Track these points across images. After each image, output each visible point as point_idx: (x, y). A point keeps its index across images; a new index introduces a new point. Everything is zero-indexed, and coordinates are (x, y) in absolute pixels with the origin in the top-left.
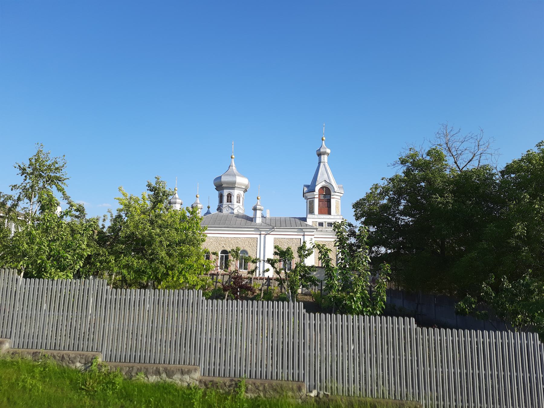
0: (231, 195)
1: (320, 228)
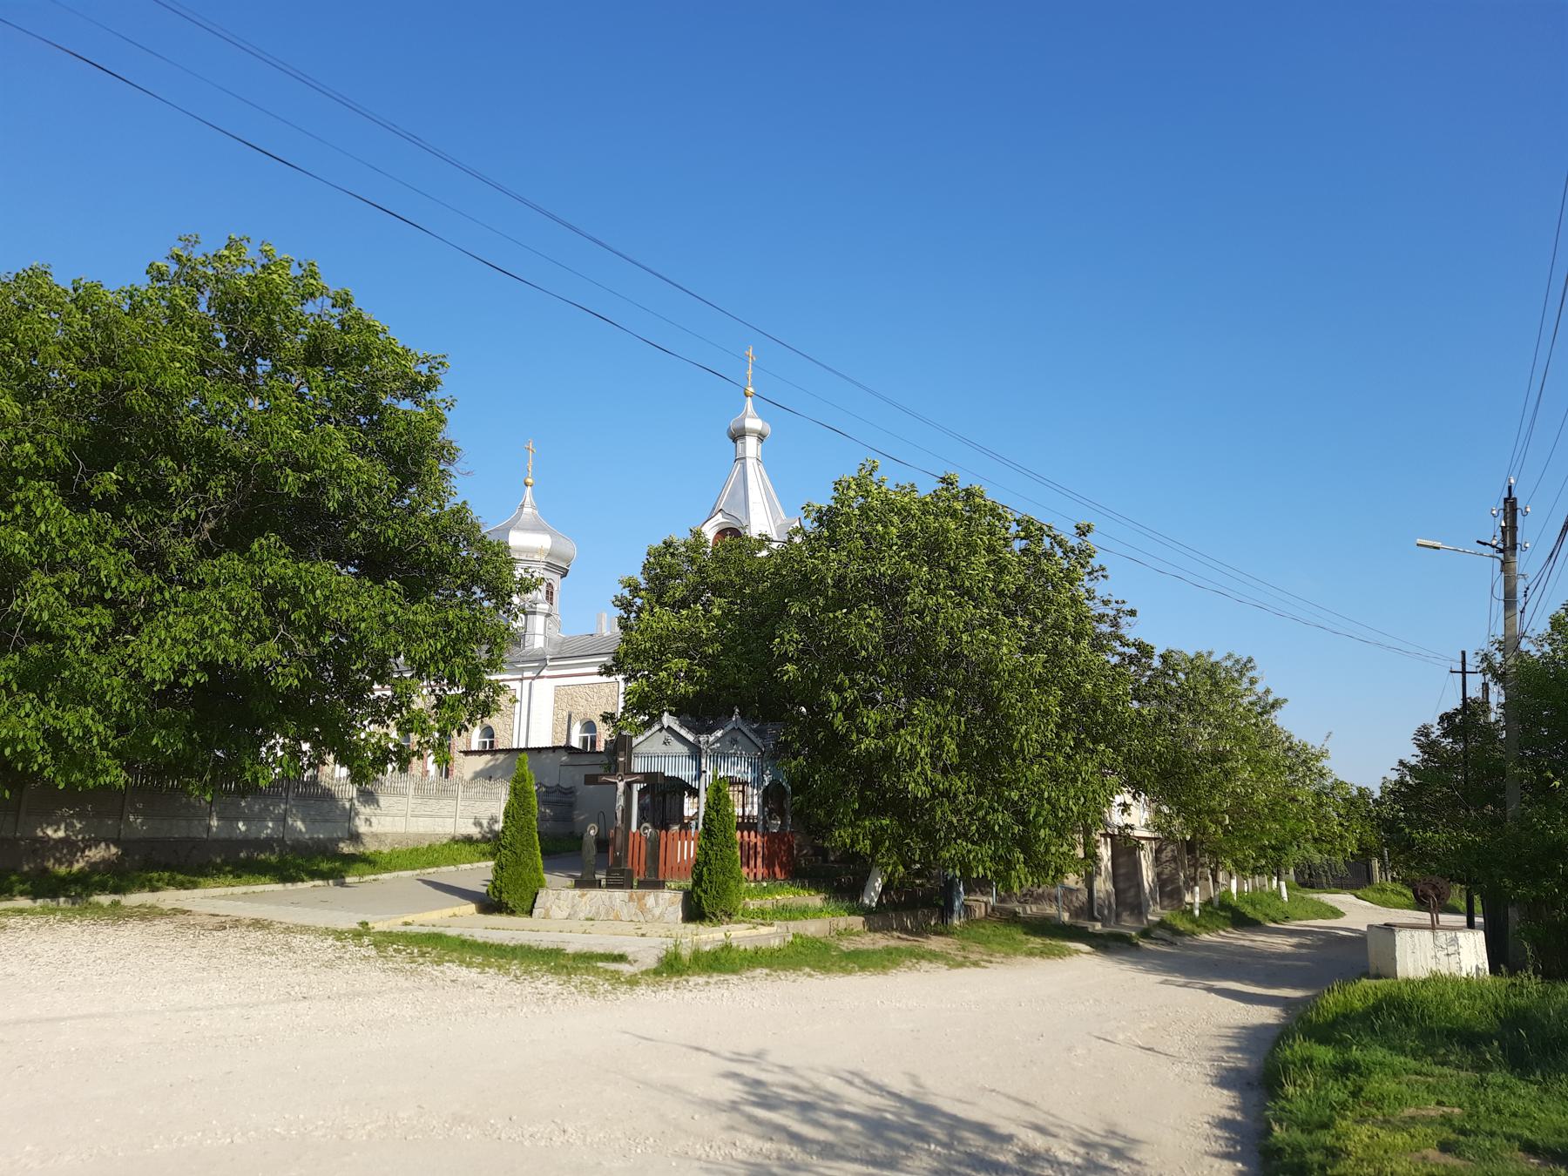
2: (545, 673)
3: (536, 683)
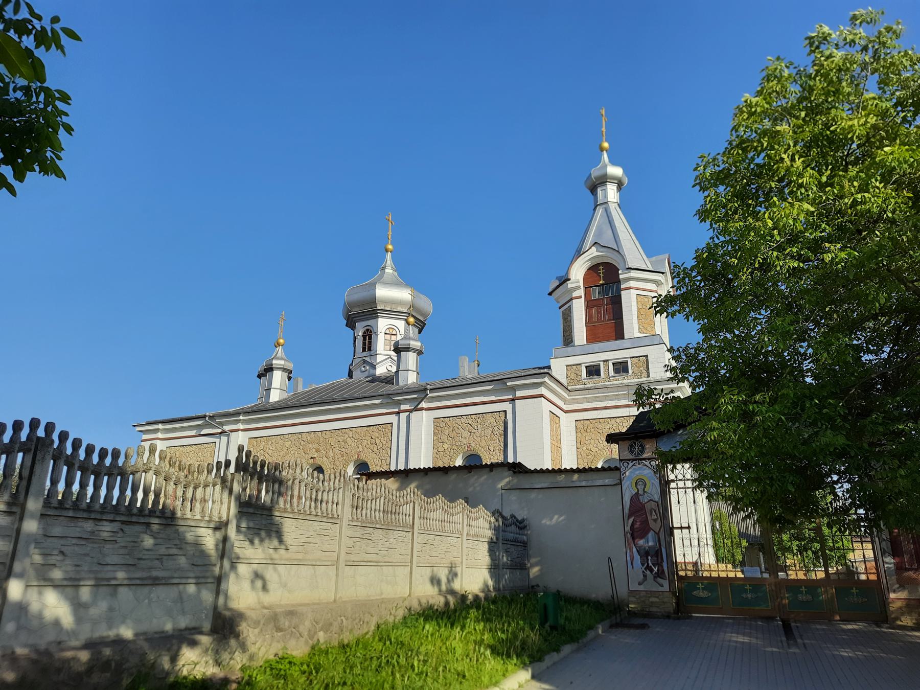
0: (371, 332)
1: (592, 382)
2: (424, 405)
3: (414, 415)
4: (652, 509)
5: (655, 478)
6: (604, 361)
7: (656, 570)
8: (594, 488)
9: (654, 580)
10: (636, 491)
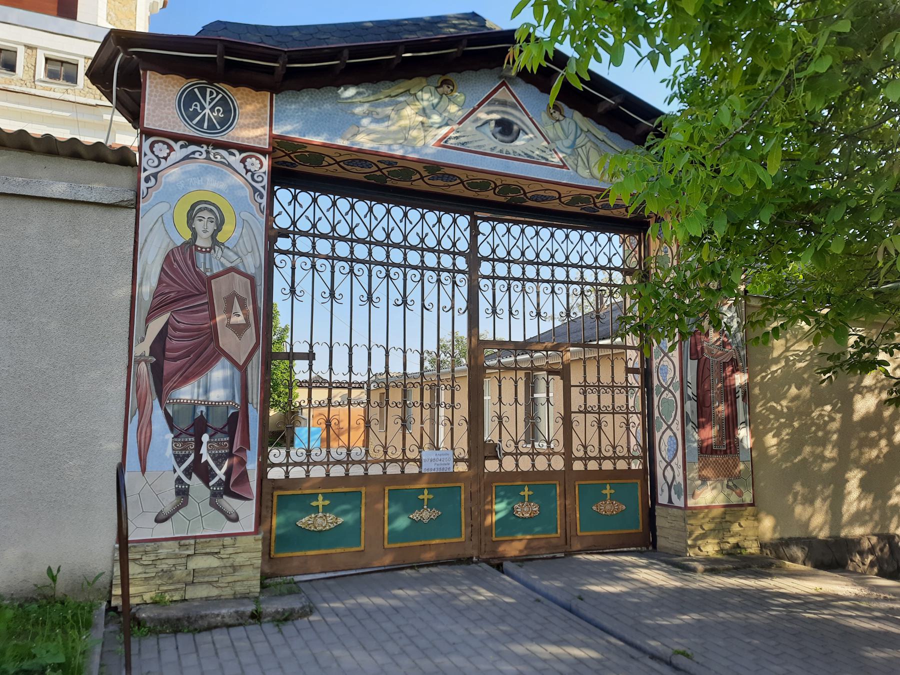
4: (234, 294)
5: (255, 209)
6: (28, 47)
7: (221, 474)
8: (28, 204)
9: (213, 504)
10: (188, 235)
